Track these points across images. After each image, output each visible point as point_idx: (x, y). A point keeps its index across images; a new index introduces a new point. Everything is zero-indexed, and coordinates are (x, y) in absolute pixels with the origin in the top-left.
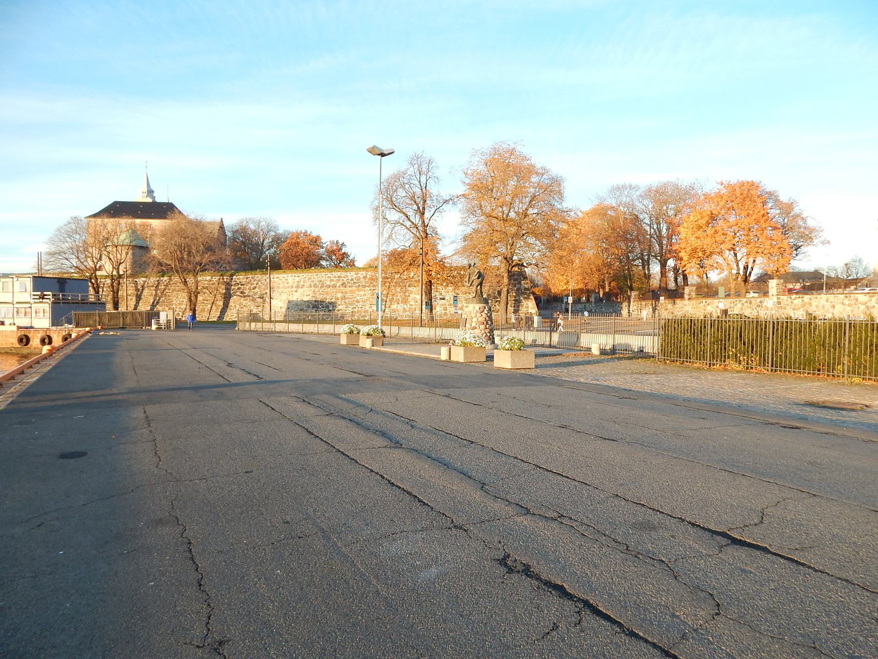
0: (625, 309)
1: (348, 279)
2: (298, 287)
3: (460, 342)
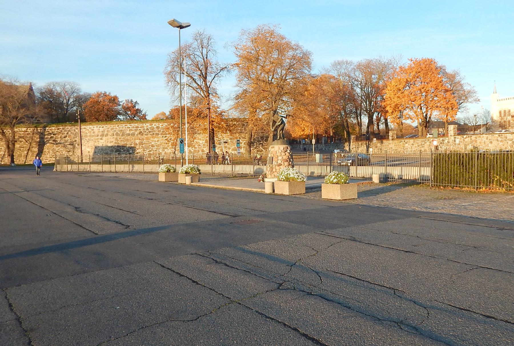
0: (347, 148)
1: (145, 129)
2: (102, 135)
3: (284, 177)
